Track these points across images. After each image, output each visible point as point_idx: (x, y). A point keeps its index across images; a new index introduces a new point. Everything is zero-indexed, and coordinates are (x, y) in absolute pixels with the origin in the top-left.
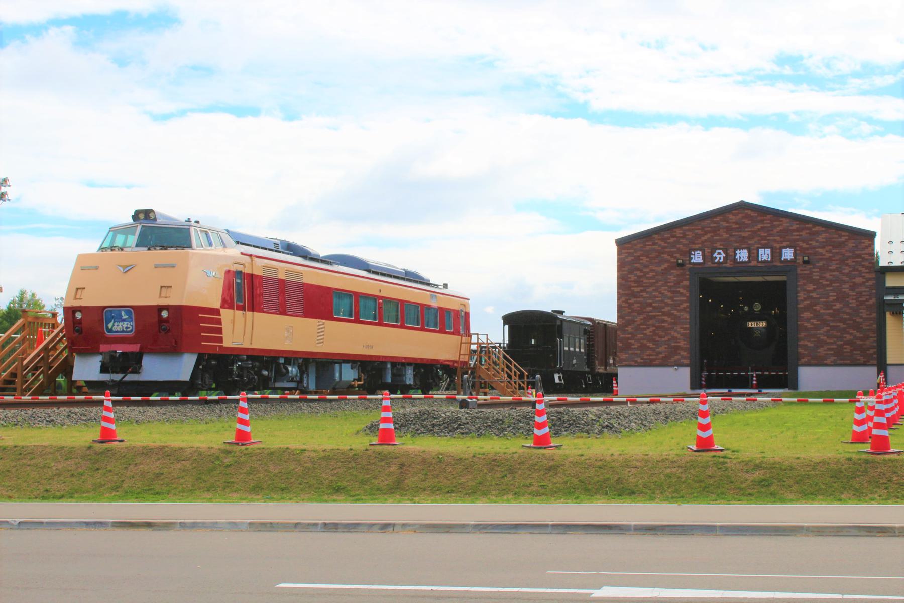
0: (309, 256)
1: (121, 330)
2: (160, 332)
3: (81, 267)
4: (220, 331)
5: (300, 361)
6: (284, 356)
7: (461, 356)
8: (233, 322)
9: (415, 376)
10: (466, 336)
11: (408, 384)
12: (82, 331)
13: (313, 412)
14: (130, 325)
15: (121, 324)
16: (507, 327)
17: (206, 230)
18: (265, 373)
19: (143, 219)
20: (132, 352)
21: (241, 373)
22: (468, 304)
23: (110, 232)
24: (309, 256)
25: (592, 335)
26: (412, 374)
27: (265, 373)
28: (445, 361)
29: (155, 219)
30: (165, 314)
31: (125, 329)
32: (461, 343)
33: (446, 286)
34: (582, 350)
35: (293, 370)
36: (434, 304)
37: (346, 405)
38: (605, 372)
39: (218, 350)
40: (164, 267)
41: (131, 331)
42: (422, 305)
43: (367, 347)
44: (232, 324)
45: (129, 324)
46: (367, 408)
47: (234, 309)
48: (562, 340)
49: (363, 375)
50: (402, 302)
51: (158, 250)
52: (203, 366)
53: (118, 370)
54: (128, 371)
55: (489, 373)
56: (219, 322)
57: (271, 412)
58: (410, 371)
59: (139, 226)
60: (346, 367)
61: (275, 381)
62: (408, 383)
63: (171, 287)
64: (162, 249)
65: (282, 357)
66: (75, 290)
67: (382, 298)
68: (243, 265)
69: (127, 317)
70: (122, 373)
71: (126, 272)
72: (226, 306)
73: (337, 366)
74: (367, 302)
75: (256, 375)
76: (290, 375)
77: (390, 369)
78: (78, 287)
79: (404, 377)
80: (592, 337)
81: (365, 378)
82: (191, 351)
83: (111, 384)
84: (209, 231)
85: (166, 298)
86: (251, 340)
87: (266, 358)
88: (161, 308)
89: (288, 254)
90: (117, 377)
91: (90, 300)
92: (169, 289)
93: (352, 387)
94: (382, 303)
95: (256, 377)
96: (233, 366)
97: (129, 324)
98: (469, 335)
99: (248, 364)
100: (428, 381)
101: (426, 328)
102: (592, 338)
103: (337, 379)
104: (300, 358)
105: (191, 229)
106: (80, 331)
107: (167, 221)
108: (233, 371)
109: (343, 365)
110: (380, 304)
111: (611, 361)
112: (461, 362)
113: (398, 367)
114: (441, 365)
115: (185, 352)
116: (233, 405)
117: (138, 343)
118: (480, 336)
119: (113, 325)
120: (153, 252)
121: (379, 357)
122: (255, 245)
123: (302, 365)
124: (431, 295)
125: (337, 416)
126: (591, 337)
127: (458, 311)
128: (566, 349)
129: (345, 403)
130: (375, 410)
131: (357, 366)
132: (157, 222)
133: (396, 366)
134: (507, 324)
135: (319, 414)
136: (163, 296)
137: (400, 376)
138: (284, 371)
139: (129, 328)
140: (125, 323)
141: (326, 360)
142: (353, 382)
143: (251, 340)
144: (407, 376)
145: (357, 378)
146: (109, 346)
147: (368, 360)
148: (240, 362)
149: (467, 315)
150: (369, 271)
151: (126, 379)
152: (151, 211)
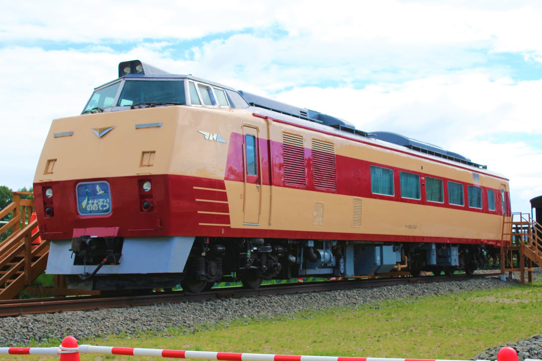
0: (341, 125)
1: (97, 209)
2: (142, 210)
3: (55, 134)
4: (225, 208)
5: (335, 244)
6: (314, 238)
7: (504, 236)
8: (244, 197)
9: (460, 256)
10: (508, 216)
11: (454, 265)
12: (53, 213)
13: (349, 304)
14: (107, 202)
15: (95, 201)
16: (534, 209)
18: (293, 259)
19: (129, 73)
20: (109, 237)
21: (258, 260)
22: (508, 184)
23: (95, 94)
24: (341, 125)
26: (457, 255)
27: (293, 259)
28: (489, 241)
29: (143, 73)
30: (147, 187)
31: (101, 209)
32: (504, 223)
33: (485, 167)
35: (325, 255)
36: (477, 183)
37: (389, 292)
39: (223, 232)
40: (148, 128)
41: (107, 211)
42: (465, 184)
43: (410, 227)
44: (242, 201)
45: (105, 201)
46: (412, 295)
49: (406, 257)
50: (445, 180)
51: (144, 108)
52: (206, 253)
54: (102, 262)
55: (534, 252)
56: (224, 196)
57: (295, 307)
58: (455, 252)
59: (122, 82)
60: (388, 250)
61: (305, 267)
62: (453, 264)
63: (154, 152)
64: (148, 107)
65: (311, 240)
66: (45, 162)
67: (424, 175)
68: (257, 128)
69: (102, 192)
72: (232, 177)
73: (378, 249)
74: (408, 178)
75: (279, 262)
76: (322, 260)
77: (435, 251)
78: (50, 159)
79: (449, 259)
81: (409, 260)
82: (183, 233)
84: (211, 87)
85: (149, 166)
86: (270, 220)
87: (291, 242)
88: (142, 179)
89: (317, 122)
90: (91, 269)
92: (152, 154)
93: (395, 270)
94: (424, 180)
95: (279, 264)
96: (247, 252)
98: (508, 213)
99: (267, 249)
100: (473, 262)
101: (470, 207)
103: (377, 262)
104: (334, 241)
105: (184, 81)
106: (51, 213)
107: (156, 75)
108: (247, 258)
109: (385, 248)
110: (422, 181)
112: (504, 241)
113: (443, 247)
114: (485, 245)
115: (177, 236)
116: (247, 300)
117: (117, 226)
118: (523, 216)
119: (88, 204)
121: (423, 238)
122: (275, 108)
123: (338, 249)
125: (378, 308)
127: (499, 191)
129: (388, 289)
130: (421, 296)
131: (400, 249)
132: (145, 76)
133: (441, 248)
134: (535, 207)
135: (357, 306)
136: (146, 164)
137: (445, 257)
138: (315, 255)
139: (106, 206)
140: (101, 200)
141: (365, 242)
142: (396, 265)
143: (270, 220)
144: (452, 257)
145: (400, 261)
146: (83, 229)
147: (412, 241)
149: (507, 194)
150: (409, 147)
152: (137, 63)
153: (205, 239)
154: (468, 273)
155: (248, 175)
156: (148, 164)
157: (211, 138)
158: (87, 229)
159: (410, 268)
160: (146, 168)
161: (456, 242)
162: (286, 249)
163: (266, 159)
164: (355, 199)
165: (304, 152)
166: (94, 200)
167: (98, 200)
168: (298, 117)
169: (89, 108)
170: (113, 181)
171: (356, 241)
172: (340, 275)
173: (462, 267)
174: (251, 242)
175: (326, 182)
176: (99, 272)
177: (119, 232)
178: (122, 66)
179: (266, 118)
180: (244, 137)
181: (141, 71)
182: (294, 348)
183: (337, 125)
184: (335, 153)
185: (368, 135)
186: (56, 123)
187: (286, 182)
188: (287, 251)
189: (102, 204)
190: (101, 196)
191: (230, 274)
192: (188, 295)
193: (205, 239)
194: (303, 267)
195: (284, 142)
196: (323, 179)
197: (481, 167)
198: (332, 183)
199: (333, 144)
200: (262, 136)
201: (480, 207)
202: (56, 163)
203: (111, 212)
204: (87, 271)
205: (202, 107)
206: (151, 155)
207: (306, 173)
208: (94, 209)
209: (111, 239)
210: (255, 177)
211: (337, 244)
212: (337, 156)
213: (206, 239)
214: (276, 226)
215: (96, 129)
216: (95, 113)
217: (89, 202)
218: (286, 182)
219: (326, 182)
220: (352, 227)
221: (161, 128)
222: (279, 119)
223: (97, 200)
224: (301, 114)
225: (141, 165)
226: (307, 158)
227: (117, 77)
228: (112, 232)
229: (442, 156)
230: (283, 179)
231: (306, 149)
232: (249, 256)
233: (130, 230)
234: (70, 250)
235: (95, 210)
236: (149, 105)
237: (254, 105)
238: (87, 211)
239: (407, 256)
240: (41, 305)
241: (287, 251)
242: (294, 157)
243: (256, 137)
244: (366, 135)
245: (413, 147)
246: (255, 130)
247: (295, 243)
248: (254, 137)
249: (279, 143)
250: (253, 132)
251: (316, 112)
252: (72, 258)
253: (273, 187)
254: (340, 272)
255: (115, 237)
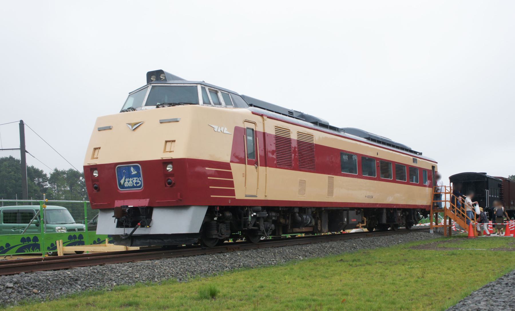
1: (132, 186)
2: (166, 186)
4: (231, 184)
8: (245, 175)
14: (139, 180)
15: (131, 180)
17: (216, 89)
20: (142, 206)
22: (437, 166)
25: (502, 187)
31: (135, 185)
34: (498, 197)
38: (509, 210)
41: (140, 186)
45: (138, 179)
47: (245, 164)
48: (488, 190)
49: (365, 218)
53: (130, 225)
56: (230, 175)
59: (149, 87)
60: (352, 213)
63: (174, 141)
64: (170, 106)
66: (92, 150)
68: (254, 123)
69: (135, 172)
70: (131, 227)
71: (134, 130)
73: (345, 212)
78: (95, 147)
80: (503, 188)
81: (367, 220)
82: (198, 204)
83: (123, 238)
85: (170, 152)
88: (165, 162)
91: (103, 159)
92: (173, 143)
96: (248, 217)
97: (138, 179)
102: (502, 189)
111: (512, 203)
118: (447, 188)
119: (125, 181)
120: (161, 109)
124: (413, 159)
126: (502, 188)
128: (490, 196)
139: (138, 183)
140: (135, 178)
146: (122, 201)
148: (255, 212)
151: (135, 233)
152: (161, 72)
153: (216, 207)
154: (407, 228)
155: (249, 159)
156: (170, 151)
157: (219, 131)
158: (125, 201)
159: (367, 226)
160: (168, 153)
161: (401, 207)
162: (278, 214)
163: (262, 147)
164: (329, 177)
165: (291, 142)
166: (130, 179)
167: (133, 178)
168: (286, 115)
169: (126, 108)
170: (145, 164)
171: (329, 207)
172: (318, 232)
173: (404, 225)
174: (251, 209)
175: (308, 164)
176: (135, 233)
177: (150, 202)
178: (150, 75)
179: (262, 115)
180: (245, 130)
181: (164, 78)
182: (147, 306)
183: (317, 122)
184: (314, 143)
185: (339, 129)
186: (99, 119)
187: (277, 164)
188: (279, 216)
189: (136, 181)
190: (135, 176)
191: (237, 232)
192: (205, 249)
193: (216, 207)
194: (290, 228)
195: (276, 134)
196: (305, 162)
197: (418, 154)
198: (312, 165)
199: (313, 136)
200: (259, 129)
201: (418, 182)
202: (100, 150)
203: (143, 188)
204: (126, 232)
205: (212, 106)
206: (172, 144)
207: (293, 157)
208: (130, 186)
209: (144, 208)
210: (253, 160)
211: (316, 210)
212: (315, 144)
213: (217, 207)
214: (271, 197)
215: (129, 124)
216: (130, 111)
217: (126, 180)
218: (277, 164)
219: (308, 164)
220: (327, 198)
221: (180, 121)
222: (272, 116)
223: (132, 179)
224: (289, 114)
225: (165, 151)
226: (294, 147)
227: (145, 83)
228: (144, 203)
229: (391, 145)
230: (275, 162)
231: (293, 139)
232: (250, 220)
233: (158, 201)
234: (113, 217)
235: (127, 187)
236: (171, 105)
237: (253, 106)
238: (125, 186)
239: (366, 218)
240: (88, 260)
241: (279, 216)
242: (283, 145)
243: (255, 130)
244: (337, 129)
245: (371, 139)
246: (254, 124)
247: (285, 209)
248: (253, 130)
249: (273, 135)
250: (252, 126)
251: (300, 112)
252: (115, 222)
253: (267, 168)
254: (318, 230)
255: (146, 207)
